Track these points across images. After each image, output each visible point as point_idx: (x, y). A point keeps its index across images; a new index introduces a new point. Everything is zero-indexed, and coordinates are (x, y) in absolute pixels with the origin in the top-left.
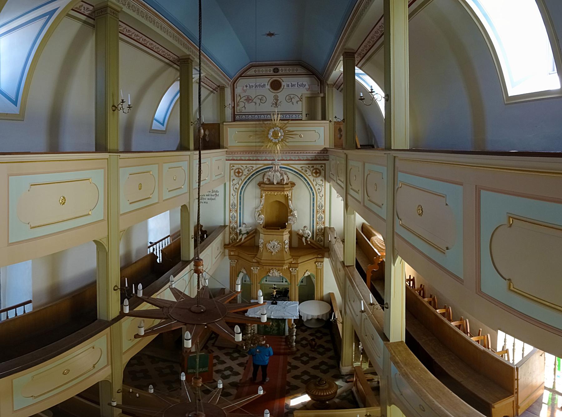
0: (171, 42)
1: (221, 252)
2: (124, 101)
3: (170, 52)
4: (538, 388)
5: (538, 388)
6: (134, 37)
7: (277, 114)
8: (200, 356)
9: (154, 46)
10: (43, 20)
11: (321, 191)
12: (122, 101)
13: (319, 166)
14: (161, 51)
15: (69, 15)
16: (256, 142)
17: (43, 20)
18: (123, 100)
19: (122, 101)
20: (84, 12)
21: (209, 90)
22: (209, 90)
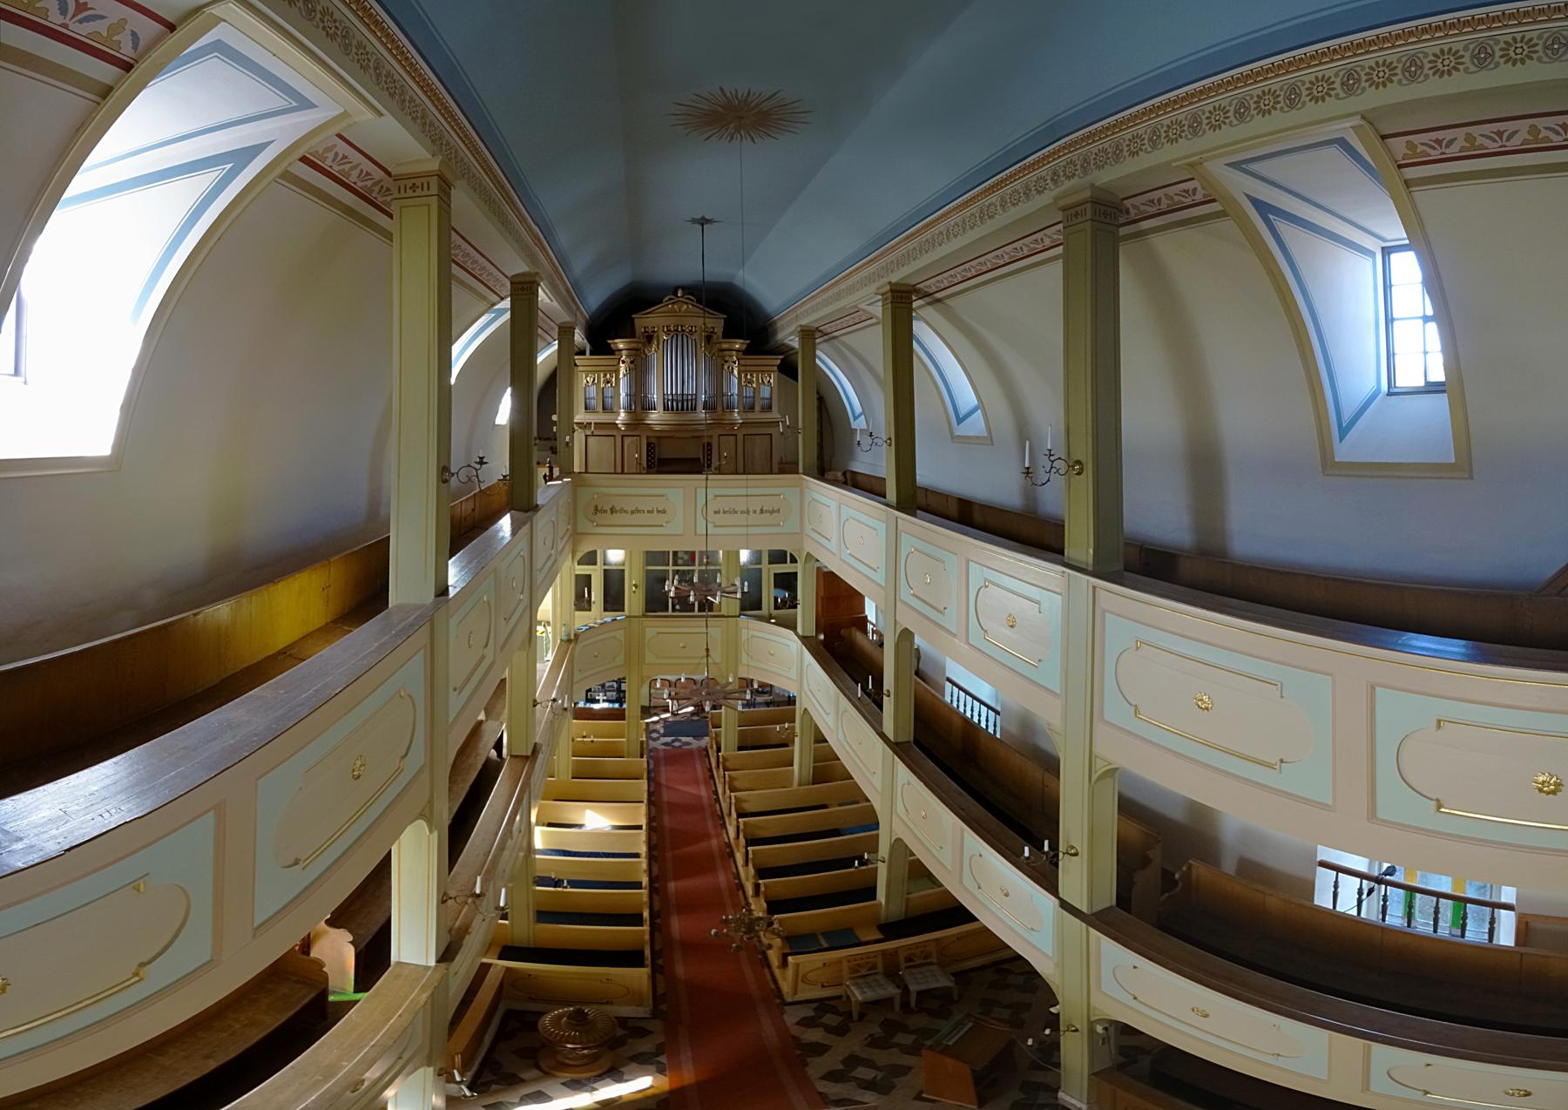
0: (1229, 596)
1: (568, 530)
2: (485, 460)
3: (945, 272)
4: (487, 951)
5: (487, 951)
6: (355, 180)
7: (675, 564)
8: (700, 571)
9: (375, 184)
10: (207, 179)
11: (613, 681)
12: (478, 460)
13: (785, 978)
14: (355, 173)
15: (276, 182)
16: (747, 526)
17: (207, 179)
18: (481, 458)
19: (478, 460)
20: (331, 167)
21: (1055, 258)
22: (1055, 258)
